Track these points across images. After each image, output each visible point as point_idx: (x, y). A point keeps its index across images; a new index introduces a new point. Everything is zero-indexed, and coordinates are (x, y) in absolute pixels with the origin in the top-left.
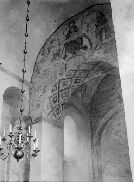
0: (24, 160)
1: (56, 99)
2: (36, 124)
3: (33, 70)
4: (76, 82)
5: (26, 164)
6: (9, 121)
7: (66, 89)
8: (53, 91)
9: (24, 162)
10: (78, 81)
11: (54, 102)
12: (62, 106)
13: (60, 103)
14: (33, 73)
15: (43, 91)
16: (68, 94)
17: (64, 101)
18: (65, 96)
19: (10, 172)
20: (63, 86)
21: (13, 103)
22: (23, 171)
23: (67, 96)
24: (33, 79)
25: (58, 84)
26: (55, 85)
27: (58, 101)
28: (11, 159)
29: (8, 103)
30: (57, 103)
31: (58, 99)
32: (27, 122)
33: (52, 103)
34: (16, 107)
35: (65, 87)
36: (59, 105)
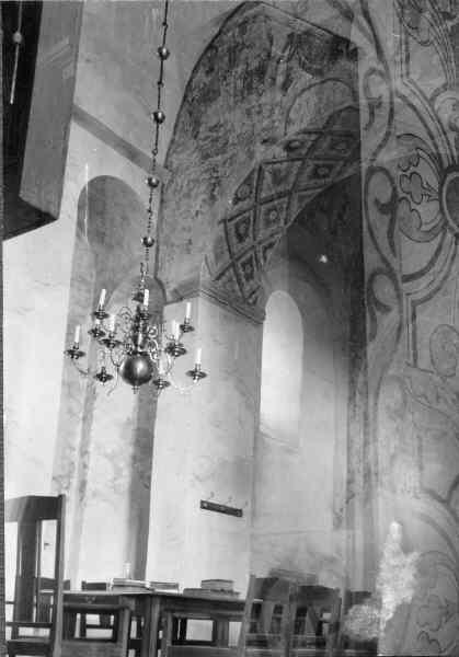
3: (176, 126)
4: (315, 174)
5: (138, 429)
8: (237, 200)
10: (322, 172)
11: (241, 238)
12: (264, 252)
14: (175, 133)
19: (91, 448)
25: (256, 175)
33: (234, 240)
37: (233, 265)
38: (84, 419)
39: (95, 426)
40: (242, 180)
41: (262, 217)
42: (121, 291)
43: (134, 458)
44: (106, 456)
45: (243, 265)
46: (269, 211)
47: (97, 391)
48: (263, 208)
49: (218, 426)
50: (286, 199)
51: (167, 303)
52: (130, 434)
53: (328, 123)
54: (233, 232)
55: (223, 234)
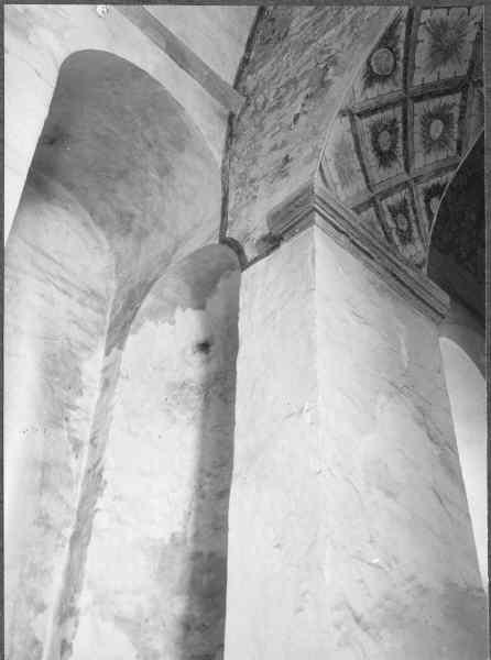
0: (189, 535)
1: (394, 146)
2: (277, 251)
3: (250, 41)
5: (196, 556)
6: (103, 312)
7: (450, 87)
8: (371, 78)
9: (189, 544)
11: (385, 158)
12: (427, 201)
13: (416, 180)
14: (248, 49)
15: (308, 91)
16: (462, 132)
17: (438, 172)
18: (442, 142)
19: (84, 600)
20: (433, 66)
21: (132, 216)
22: (177, 607)
23: (454, 145)
24: (249, 77)
25: (402, 32)
26: (388, 40)
27: (401, 160)
28: (97, 516)
29: (102, 224)
30: (398, 167)
31: (405, 147)
32: (210, 303)
34: (147, 234)
35: (448, 71)
36: (406, 184)
37: (372, 202)
38: (75, 538)
39: (92, 549)
40: (377, 39)
41: (418, 128)
42: (160, 296)
43: (187, 625)
44: (120, 620)
45: (394, 212)
46: (429, 118)
47: (105, 475)
48: (420, 109)
49: (389, 494)
50: (458, 96)
51: (244, 265)
52: (179, 569)
53: (436, 443)
54: (367, 143)
55: (350, 138)
